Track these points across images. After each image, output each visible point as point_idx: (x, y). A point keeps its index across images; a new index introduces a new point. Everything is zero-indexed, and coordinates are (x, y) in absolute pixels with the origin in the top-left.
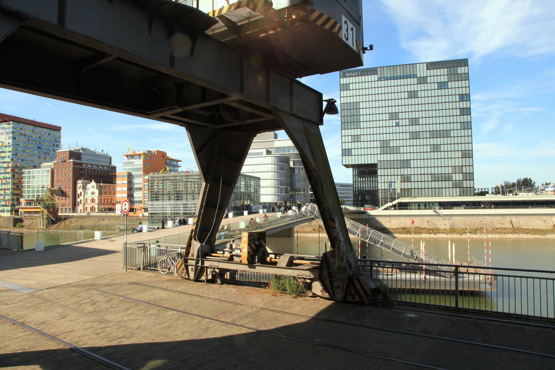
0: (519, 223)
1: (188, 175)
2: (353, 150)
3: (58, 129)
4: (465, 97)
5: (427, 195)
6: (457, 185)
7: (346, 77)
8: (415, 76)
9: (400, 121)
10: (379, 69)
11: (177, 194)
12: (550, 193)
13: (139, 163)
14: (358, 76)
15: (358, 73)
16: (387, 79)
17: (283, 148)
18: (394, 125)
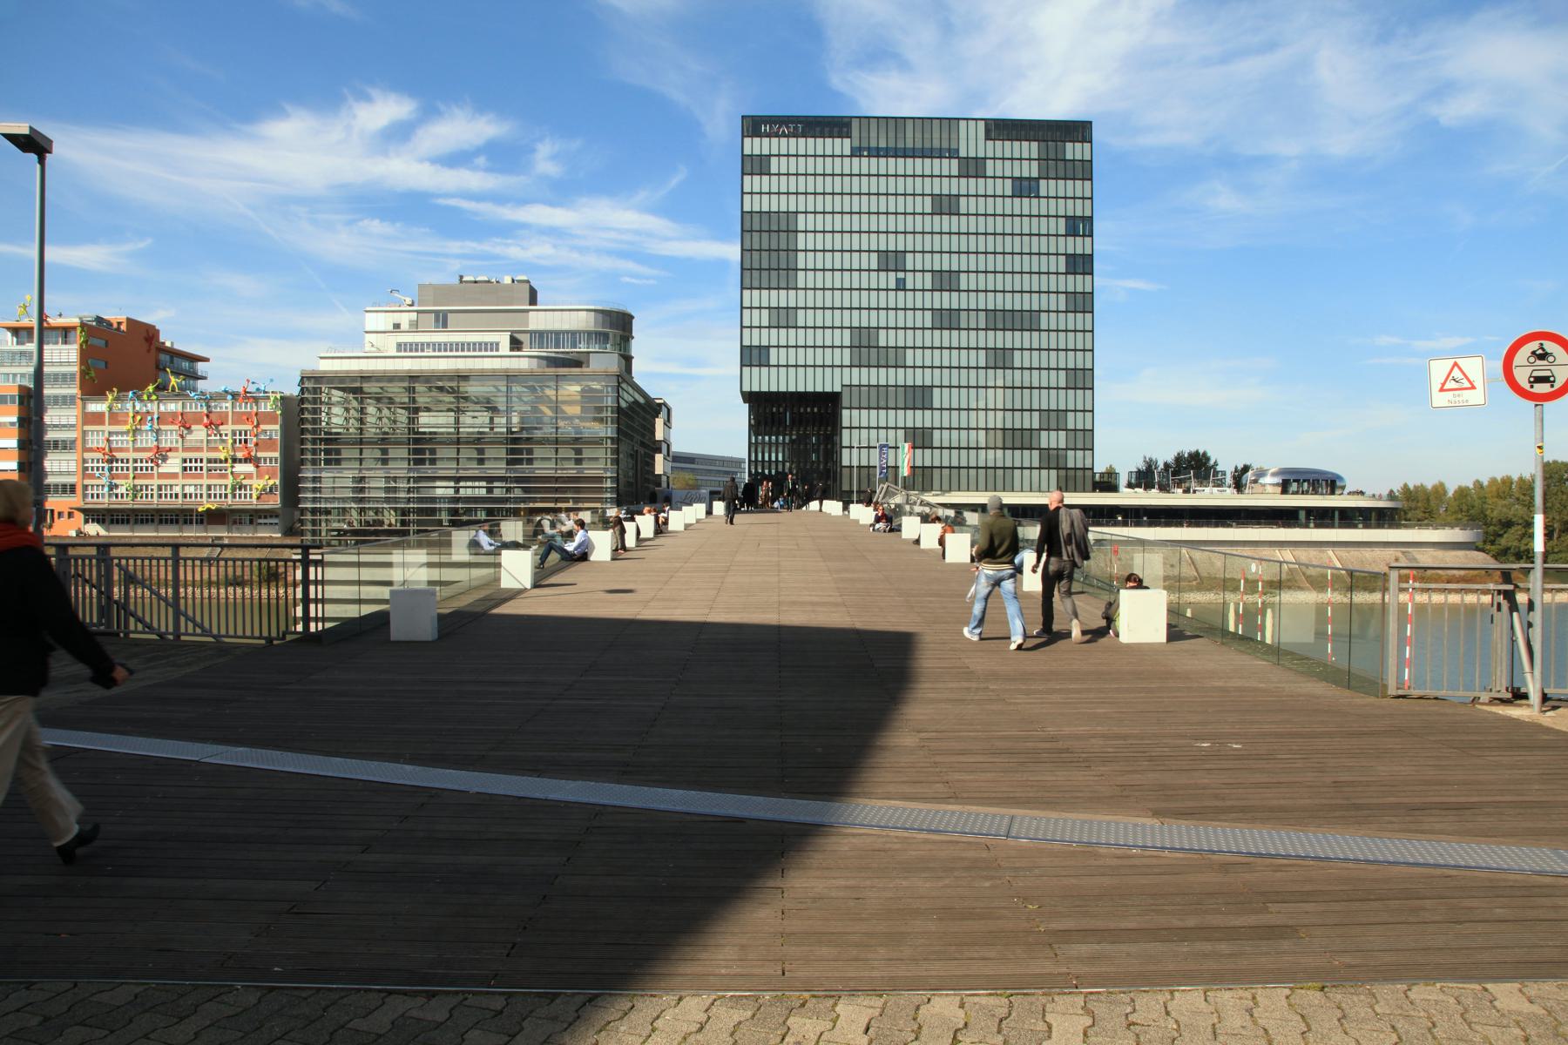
0: (1212, 564)
2: (773, 351)
4: (1080, 226)
5: (973, 486)
6: (1052, 460)
7: (760, 135)
8: (953, 154)
9: (910, 276)
10: (855, 124)
11: (416, 441)
12: (1269, 489)
13: (64, 357)
14: (796, 136)
16: (877, 153)
17: (557, 333)
18: (892, 285)
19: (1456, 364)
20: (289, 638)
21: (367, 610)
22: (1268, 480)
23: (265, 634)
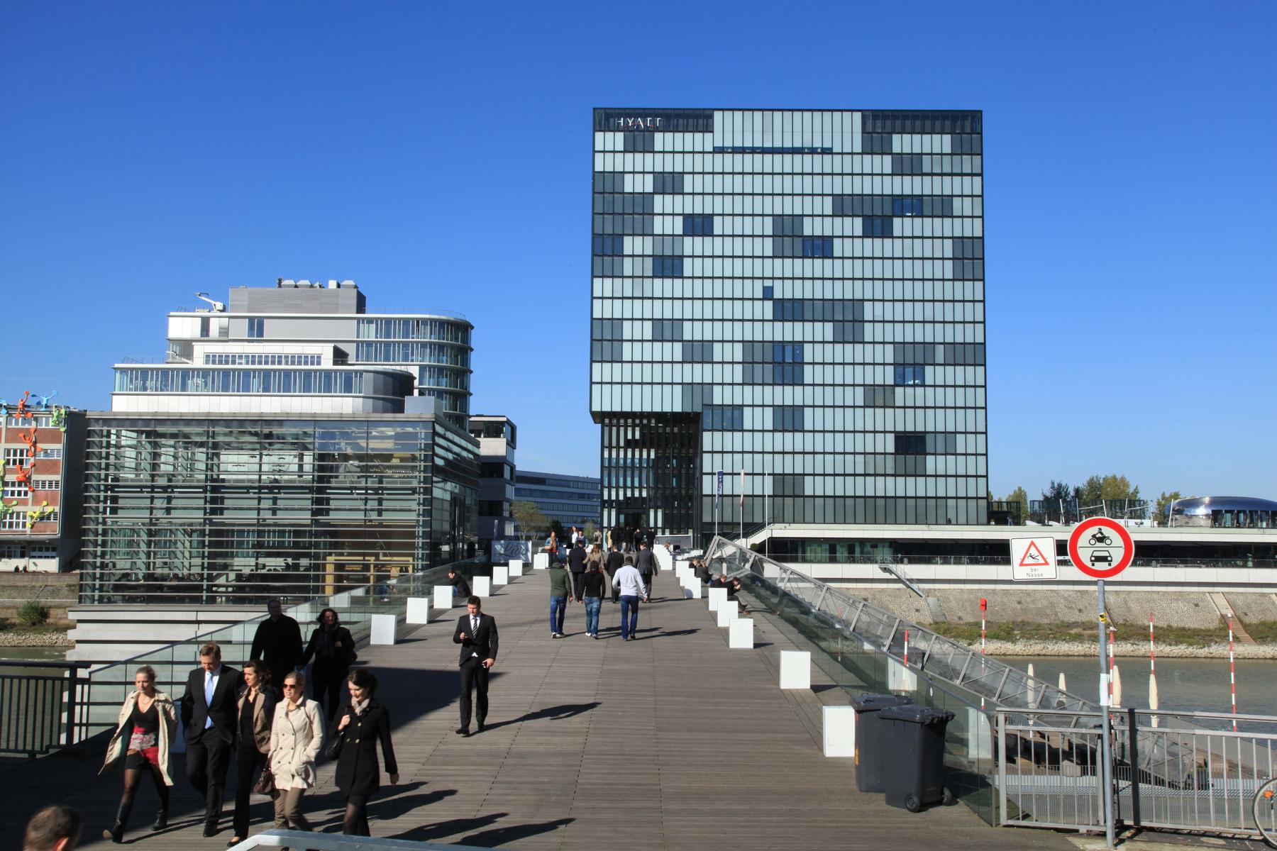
0: (1129, 609)
1: (837, 763)
3: (472, 328)
9: (778, 284)
15: (653, 122)
19: (1032, 543)
20: (52, 751)
22: (1202, 511)
23: (29, 747)
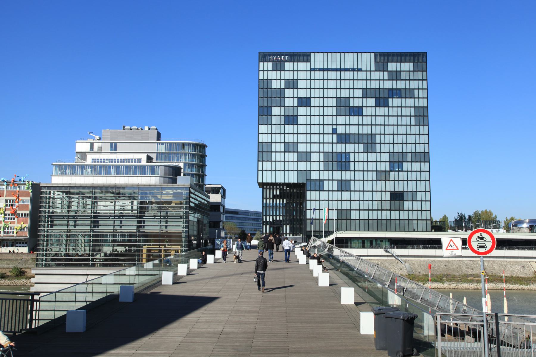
0: (494, 268)
19: (451, 240)
20: (23, 332)
21: (59, 314)
23: (13, 330)
